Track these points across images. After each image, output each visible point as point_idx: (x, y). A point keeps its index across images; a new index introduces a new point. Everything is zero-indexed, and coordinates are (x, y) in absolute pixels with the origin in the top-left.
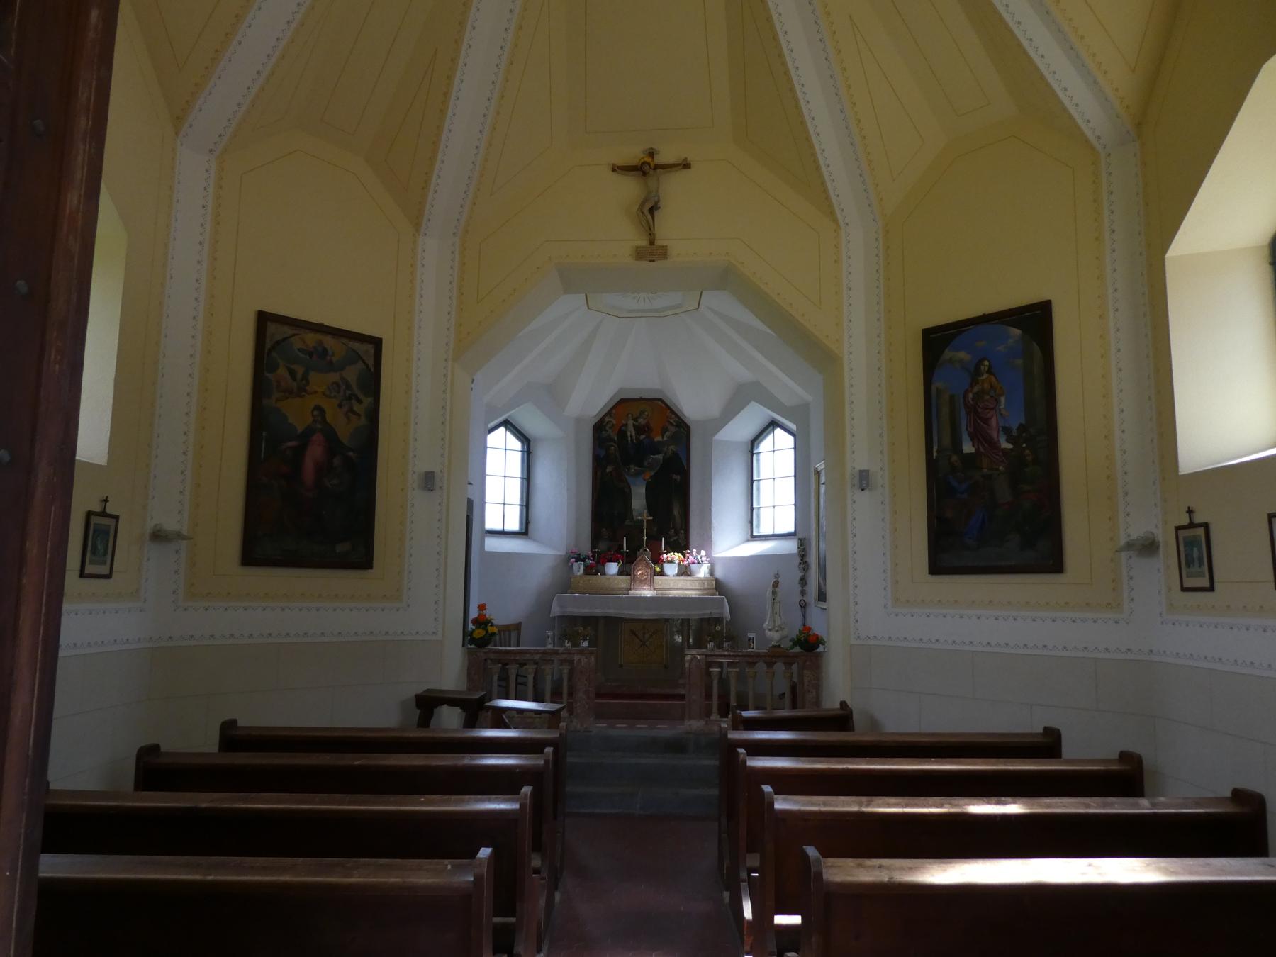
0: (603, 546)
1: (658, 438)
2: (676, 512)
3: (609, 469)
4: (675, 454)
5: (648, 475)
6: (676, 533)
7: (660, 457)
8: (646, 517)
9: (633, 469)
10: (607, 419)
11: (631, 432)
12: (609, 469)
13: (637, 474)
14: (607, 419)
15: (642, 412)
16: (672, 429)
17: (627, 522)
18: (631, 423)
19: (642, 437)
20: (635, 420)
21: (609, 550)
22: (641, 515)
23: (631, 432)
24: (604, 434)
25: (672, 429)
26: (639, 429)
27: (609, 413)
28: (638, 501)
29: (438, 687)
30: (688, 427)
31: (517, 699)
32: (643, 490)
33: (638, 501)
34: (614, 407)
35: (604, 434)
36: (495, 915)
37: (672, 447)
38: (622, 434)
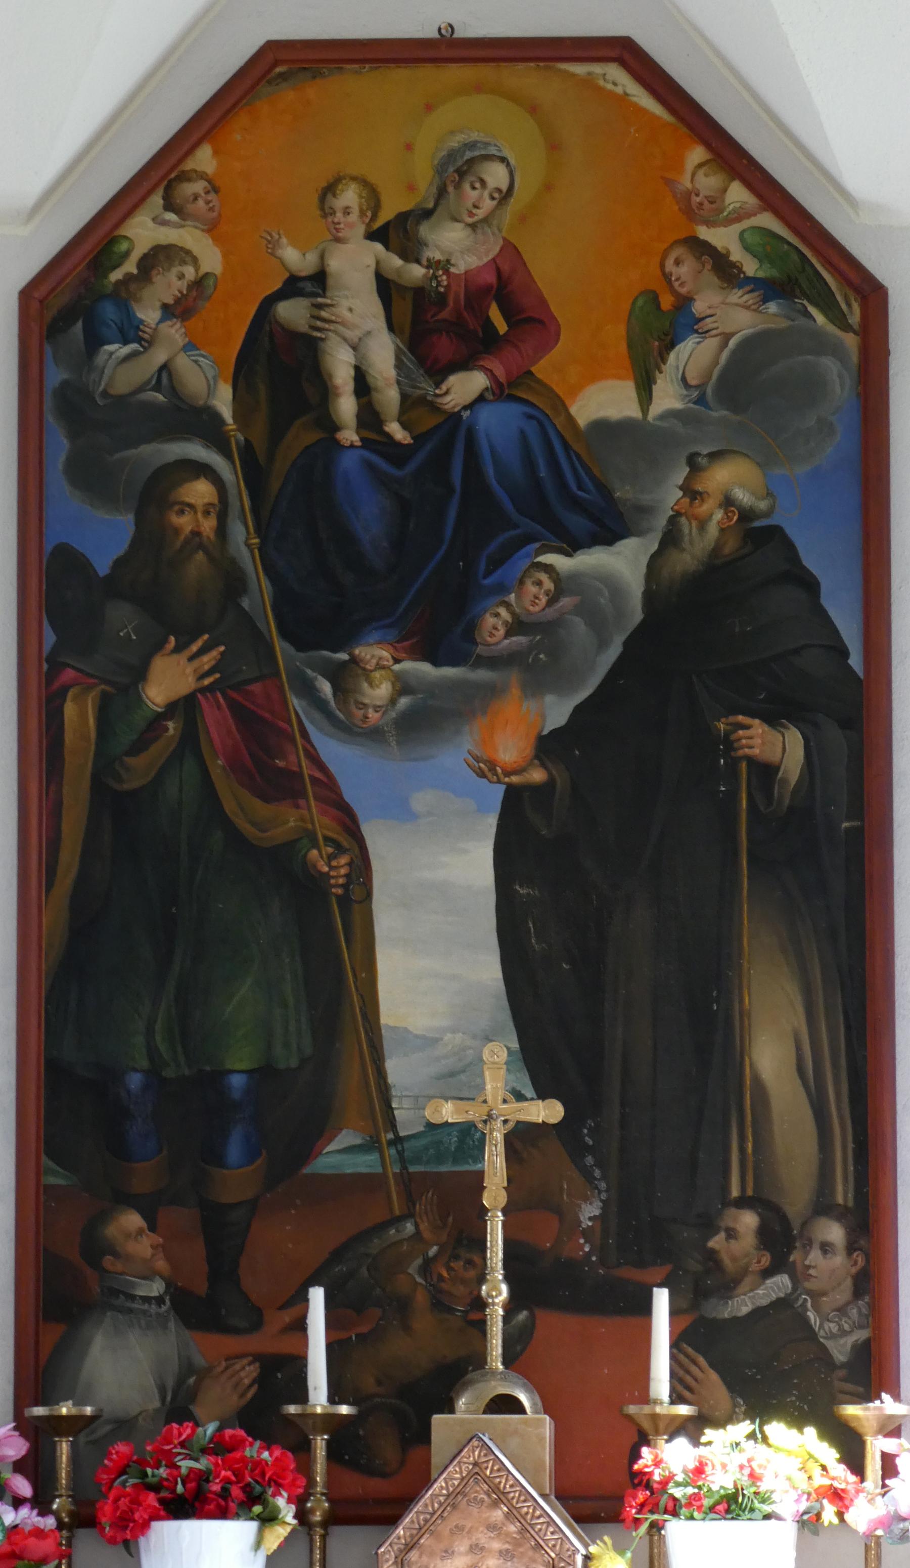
0: (120, 1369)
1: (605, 401)
2: (773, 1051)
3: (169, 679)
4: (759, 536)
5: (518, 727)
6: (780, 1242)
7: (622, 564)
8: (501, 1099)
9: (384, 671)
10: (144, 231)
11: (361, 346)
12: (169, 679)
13: (421, 722)
14: (144, 231)
15: (460, 167)
16: (735, 316)
17: (340, 1153)
18: (356, 263)
19: (464, 387)
20: (399, 234)
21: (179, 1408)
22: (460, 1079)
23: (361, 346)
24: (121, 369)
25: (735, 316)
26: (435, 325)
27: (161, 176)
28: (435, 964)
29: (355, 809)
30: (872, 294)
31: (329, 1347)
32: (470, 865)
33: (435, 964)
34: (211, 120)
35: (121, 369)
36: (782, 1304)
37: (734, 479)
38: (281, 365)
